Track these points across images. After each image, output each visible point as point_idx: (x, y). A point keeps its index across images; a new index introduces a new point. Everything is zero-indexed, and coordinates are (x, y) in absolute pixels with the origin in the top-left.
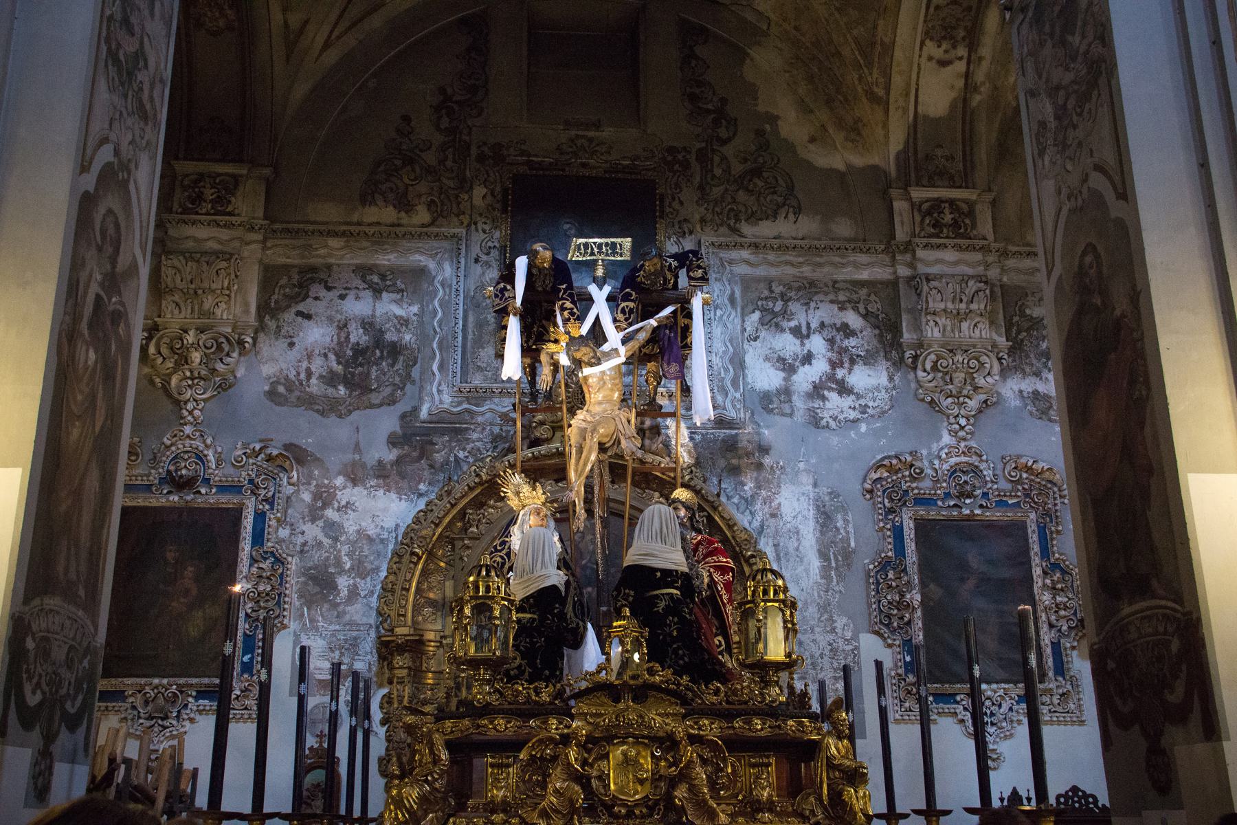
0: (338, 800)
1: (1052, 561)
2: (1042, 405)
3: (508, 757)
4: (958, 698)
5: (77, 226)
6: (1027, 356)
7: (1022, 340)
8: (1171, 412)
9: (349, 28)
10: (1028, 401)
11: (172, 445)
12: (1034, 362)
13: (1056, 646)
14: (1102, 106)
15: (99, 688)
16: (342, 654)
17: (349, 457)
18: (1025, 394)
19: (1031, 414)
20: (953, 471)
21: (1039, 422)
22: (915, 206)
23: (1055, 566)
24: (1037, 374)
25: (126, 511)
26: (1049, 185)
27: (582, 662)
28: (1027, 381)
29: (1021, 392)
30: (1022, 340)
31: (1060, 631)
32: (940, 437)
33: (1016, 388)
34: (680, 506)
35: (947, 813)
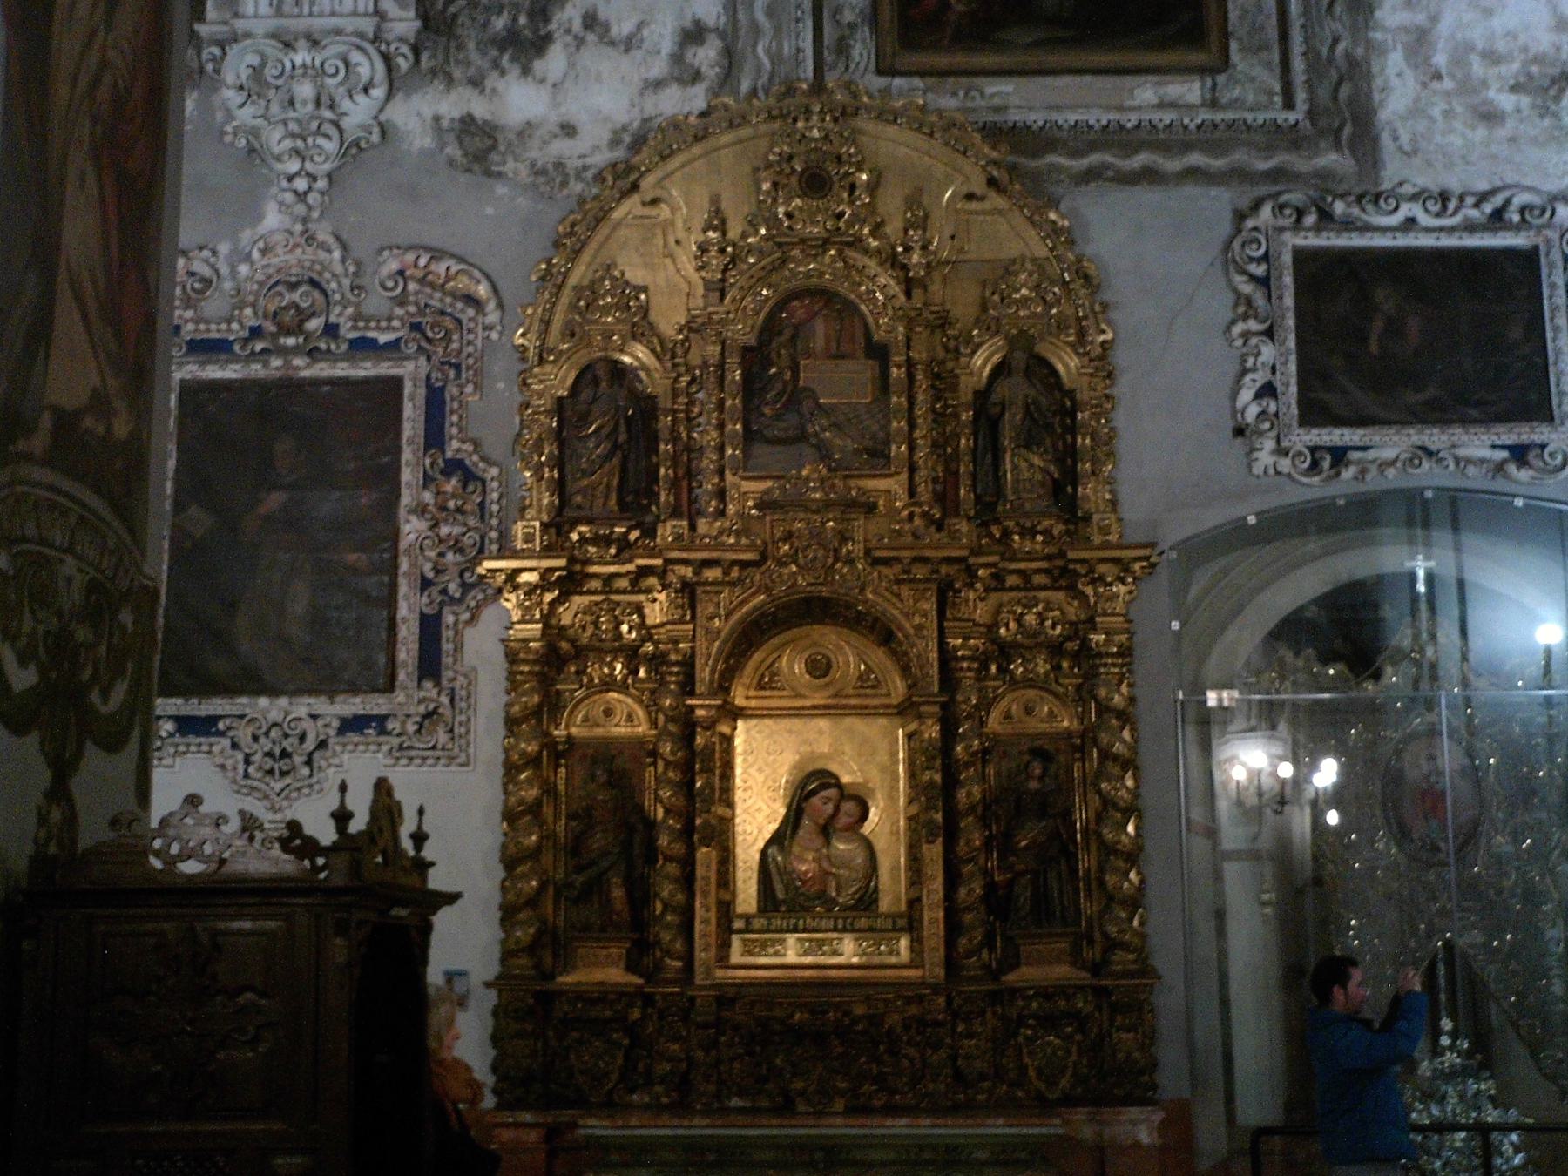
0: (728, 1137)
1: (449, 454)
2: (478, 143)
3: (475, 464)
4: (221, 726)
5: (52, 313)
6: (460, 48)
7: (455, 16)
8: (1289, 610)
9: (734, 144)
10: (451, 138)
11: (451, 365)
12: (475, 57)
13: (898, 560)
14: (842, 48)
15: (178, 375)
16: (960, 591)
17: (1512, 468)
18: (445, 124)
19: (451, 163)
20: (273, 286)
21: (463, 178)
22: (898, 954)
23: (455, 466)
24: (476, 83)
25: (397, 382)
26: (684, 258)
27: (177, 234)
28: (454, 96)
29: (437, 119)
30: (455, 16)
31: (444, 591)
32: (260, 217)
33: (428, 113)
34: (1026, 642)
35: (452, 898)
